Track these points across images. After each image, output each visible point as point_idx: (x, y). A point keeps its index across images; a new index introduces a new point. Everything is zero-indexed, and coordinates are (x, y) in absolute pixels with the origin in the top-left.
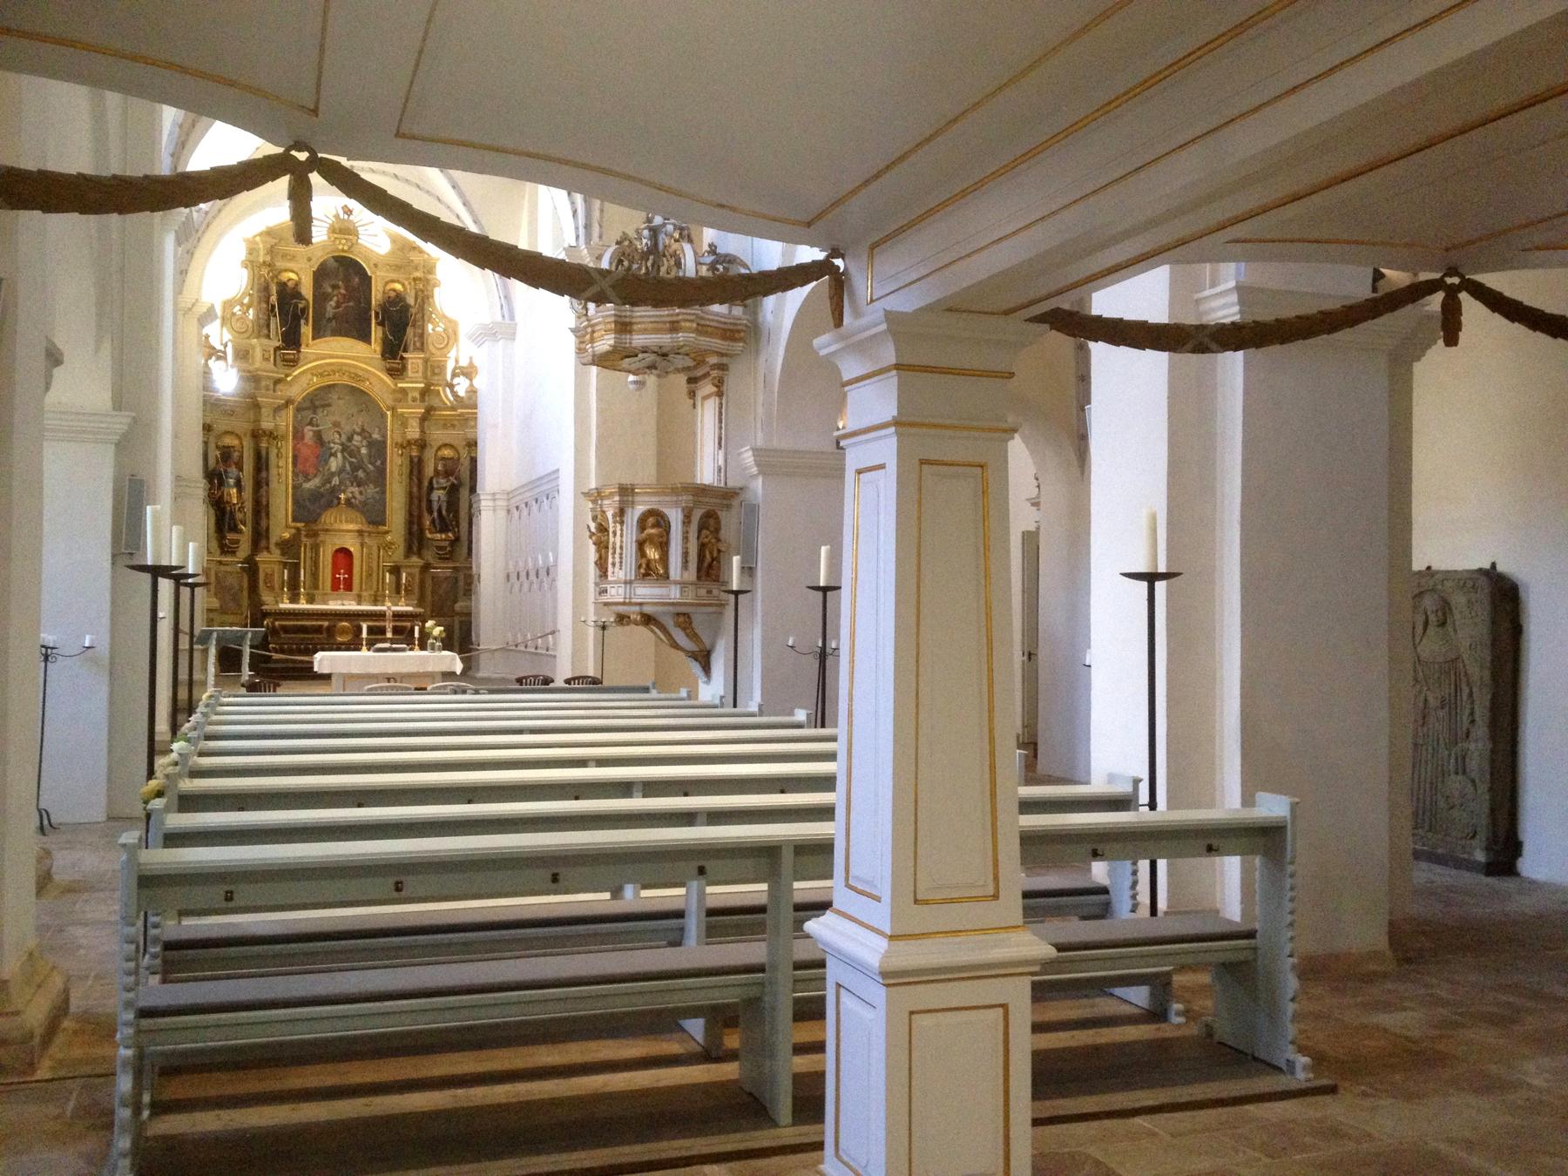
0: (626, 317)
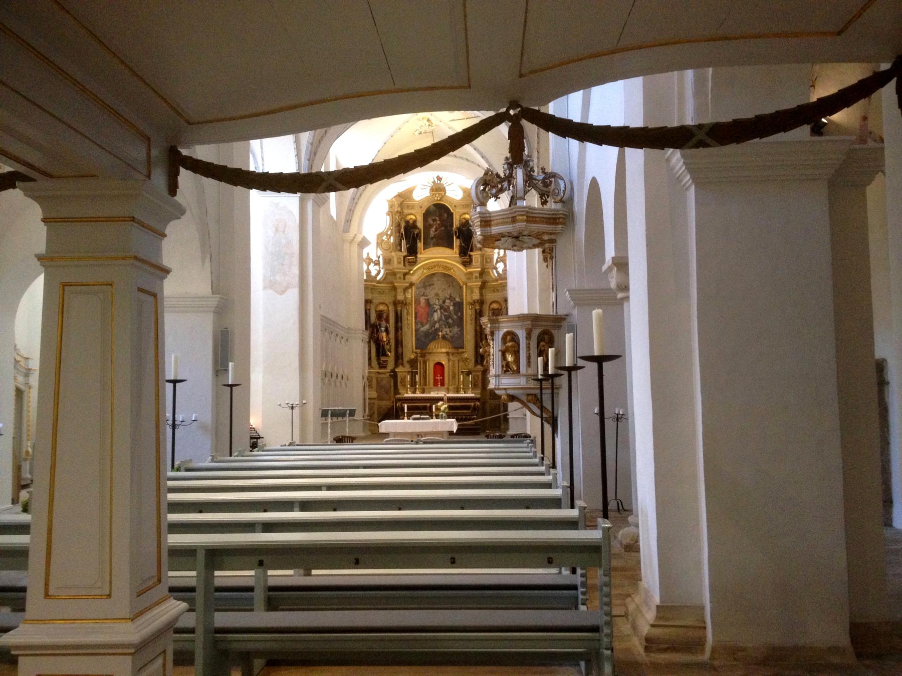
0: (487, 217)
